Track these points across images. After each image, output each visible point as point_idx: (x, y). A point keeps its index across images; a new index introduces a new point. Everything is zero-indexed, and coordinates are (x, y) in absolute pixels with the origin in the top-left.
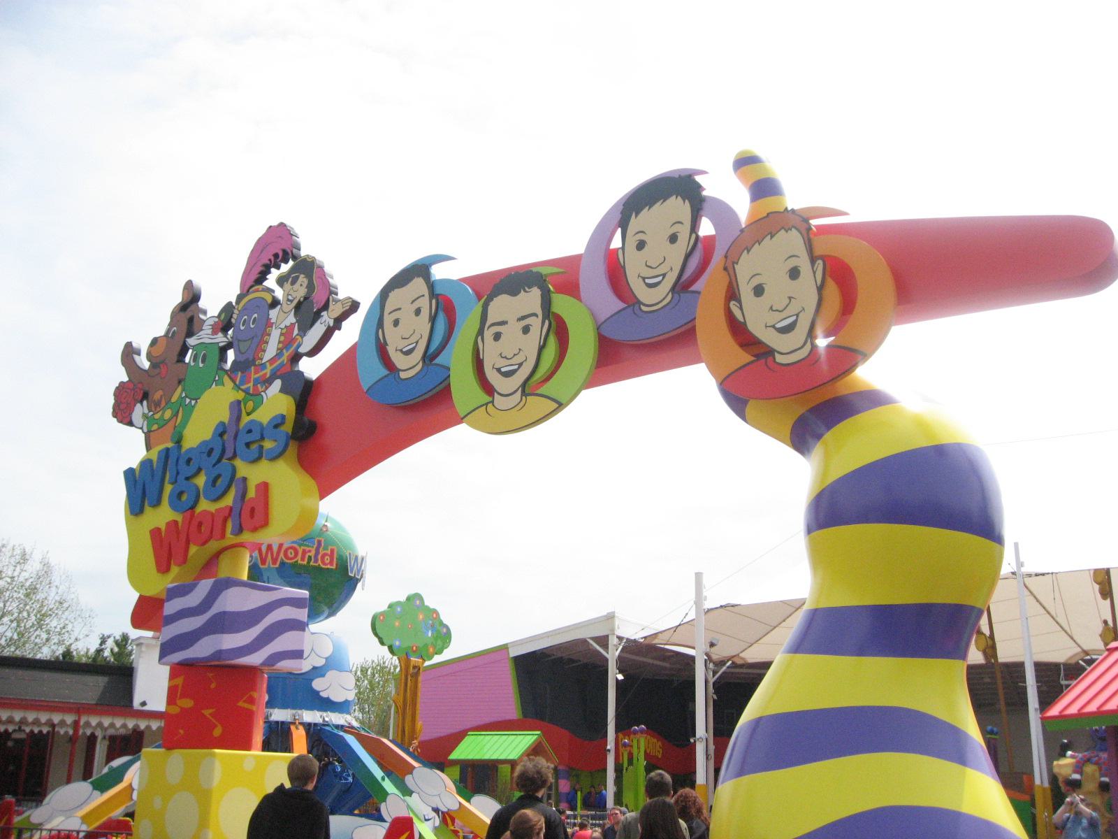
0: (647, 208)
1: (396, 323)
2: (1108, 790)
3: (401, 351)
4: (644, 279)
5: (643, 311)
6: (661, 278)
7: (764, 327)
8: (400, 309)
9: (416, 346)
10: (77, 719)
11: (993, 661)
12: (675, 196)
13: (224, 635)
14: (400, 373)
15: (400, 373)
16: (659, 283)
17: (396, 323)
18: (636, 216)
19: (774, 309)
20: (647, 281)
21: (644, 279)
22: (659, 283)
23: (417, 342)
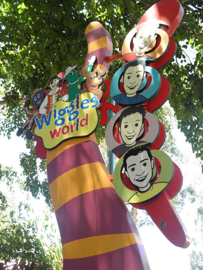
0: (124, 117)
1: (129, 78)
2: (11, 39)
3: (129, 87)
4: (127, 137)
5: (126, 146)
6: (132, 137)
7: (134, 180)
8: (131, 73)
9: (135, 87)
10: (110, 58)
11: (34, 159)
12: (145, 114)
13: (96, 163)
14: (127, 94)
15: (127, 94)
16: (132, 138)
17: (129, 78)
18: (125, 118)
19: (137, 175)
20: (128, 137)
21: (127, 137)
22: (132, 138)
23: (136, 86)
